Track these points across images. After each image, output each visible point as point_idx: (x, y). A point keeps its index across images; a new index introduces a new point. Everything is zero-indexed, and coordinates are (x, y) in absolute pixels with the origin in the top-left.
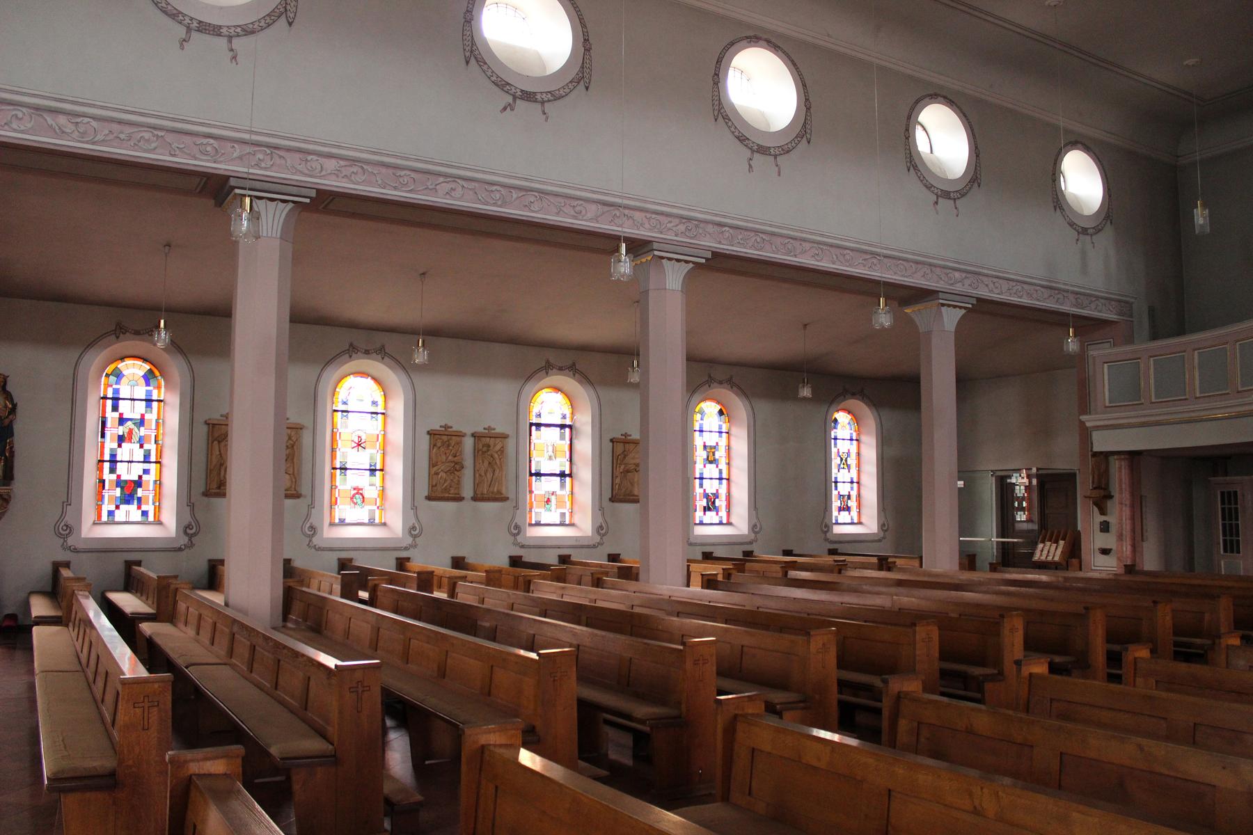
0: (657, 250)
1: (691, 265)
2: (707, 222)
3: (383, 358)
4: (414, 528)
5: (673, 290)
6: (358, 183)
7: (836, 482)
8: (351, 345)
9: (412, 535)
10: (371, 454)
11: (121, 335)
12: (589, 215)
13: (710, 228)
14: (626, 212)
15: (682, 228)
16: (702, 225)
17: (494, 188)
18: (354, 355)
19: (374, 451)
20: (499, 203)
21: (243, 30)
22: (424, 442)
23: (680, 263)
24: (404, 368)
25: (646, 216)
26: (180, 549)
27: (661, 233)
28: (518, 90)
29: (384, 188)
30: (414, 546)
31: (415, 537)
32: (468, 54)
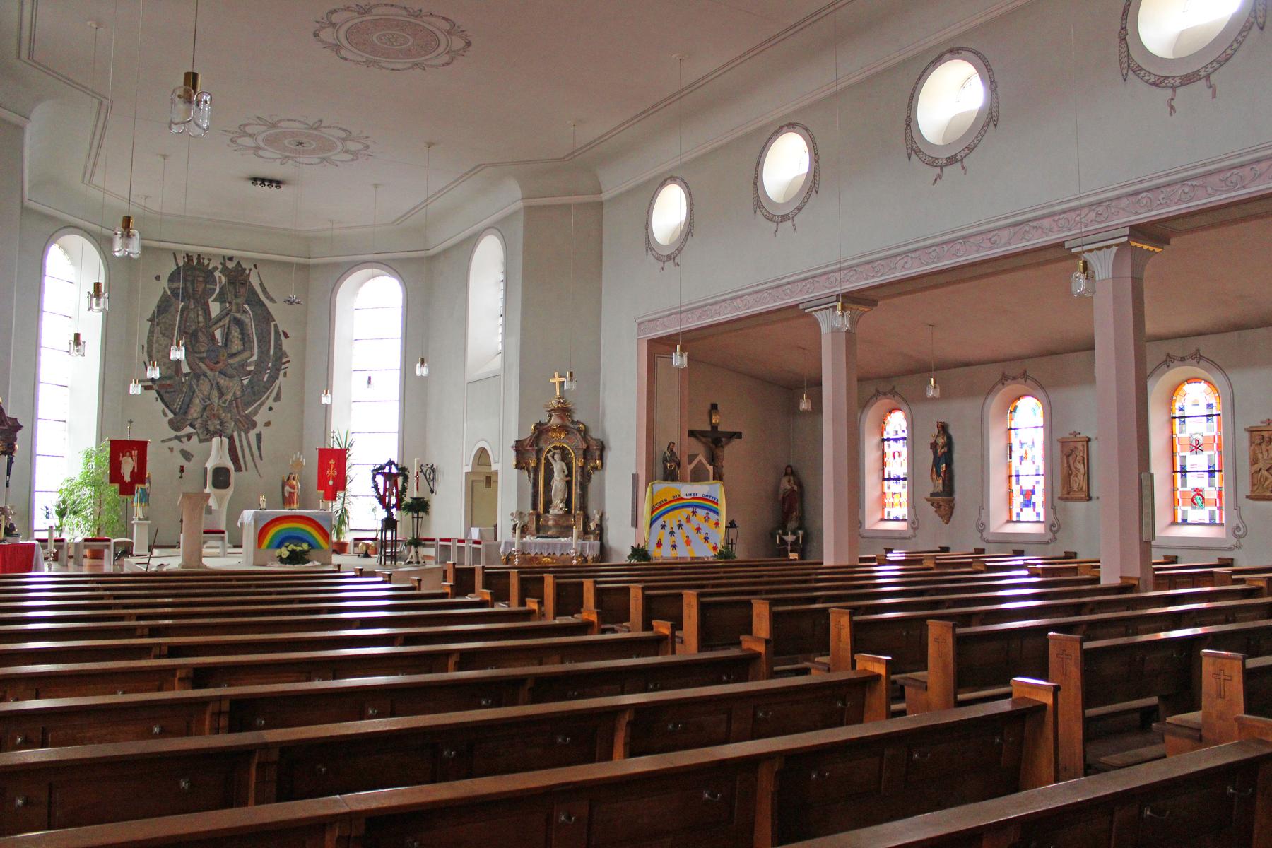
0: (1074, 247)
1: (1115, 249)
2: (1118, 198)
3: (1198, 362)
4: (1238, 528)
5: (1104, 280)
6: (854, 282)
7: (1017, 476)
8: (1168, 355)
9: (1236, 536)
10: (1209, 456)
11: (1171, 363)
12: (1003, 241)
13: (1124, 202)
14: (1035, 224)
15: (1092, 215)
16: (1114, 203)
17: (931, 250)
18: (1006, 383)
19: (1211, 453)
20: (935, 260)
21: (1218, 62)
22: (1244, 439)
23: (1102, 251)
24: (1219, 368)
25: (1054, 220)
26: (1047, 543)
27: (1070, 230)
28: (944, 160)
29: (867, 279)
30: (1238, 547)
31: (1239, 537)
32: (909, 151)
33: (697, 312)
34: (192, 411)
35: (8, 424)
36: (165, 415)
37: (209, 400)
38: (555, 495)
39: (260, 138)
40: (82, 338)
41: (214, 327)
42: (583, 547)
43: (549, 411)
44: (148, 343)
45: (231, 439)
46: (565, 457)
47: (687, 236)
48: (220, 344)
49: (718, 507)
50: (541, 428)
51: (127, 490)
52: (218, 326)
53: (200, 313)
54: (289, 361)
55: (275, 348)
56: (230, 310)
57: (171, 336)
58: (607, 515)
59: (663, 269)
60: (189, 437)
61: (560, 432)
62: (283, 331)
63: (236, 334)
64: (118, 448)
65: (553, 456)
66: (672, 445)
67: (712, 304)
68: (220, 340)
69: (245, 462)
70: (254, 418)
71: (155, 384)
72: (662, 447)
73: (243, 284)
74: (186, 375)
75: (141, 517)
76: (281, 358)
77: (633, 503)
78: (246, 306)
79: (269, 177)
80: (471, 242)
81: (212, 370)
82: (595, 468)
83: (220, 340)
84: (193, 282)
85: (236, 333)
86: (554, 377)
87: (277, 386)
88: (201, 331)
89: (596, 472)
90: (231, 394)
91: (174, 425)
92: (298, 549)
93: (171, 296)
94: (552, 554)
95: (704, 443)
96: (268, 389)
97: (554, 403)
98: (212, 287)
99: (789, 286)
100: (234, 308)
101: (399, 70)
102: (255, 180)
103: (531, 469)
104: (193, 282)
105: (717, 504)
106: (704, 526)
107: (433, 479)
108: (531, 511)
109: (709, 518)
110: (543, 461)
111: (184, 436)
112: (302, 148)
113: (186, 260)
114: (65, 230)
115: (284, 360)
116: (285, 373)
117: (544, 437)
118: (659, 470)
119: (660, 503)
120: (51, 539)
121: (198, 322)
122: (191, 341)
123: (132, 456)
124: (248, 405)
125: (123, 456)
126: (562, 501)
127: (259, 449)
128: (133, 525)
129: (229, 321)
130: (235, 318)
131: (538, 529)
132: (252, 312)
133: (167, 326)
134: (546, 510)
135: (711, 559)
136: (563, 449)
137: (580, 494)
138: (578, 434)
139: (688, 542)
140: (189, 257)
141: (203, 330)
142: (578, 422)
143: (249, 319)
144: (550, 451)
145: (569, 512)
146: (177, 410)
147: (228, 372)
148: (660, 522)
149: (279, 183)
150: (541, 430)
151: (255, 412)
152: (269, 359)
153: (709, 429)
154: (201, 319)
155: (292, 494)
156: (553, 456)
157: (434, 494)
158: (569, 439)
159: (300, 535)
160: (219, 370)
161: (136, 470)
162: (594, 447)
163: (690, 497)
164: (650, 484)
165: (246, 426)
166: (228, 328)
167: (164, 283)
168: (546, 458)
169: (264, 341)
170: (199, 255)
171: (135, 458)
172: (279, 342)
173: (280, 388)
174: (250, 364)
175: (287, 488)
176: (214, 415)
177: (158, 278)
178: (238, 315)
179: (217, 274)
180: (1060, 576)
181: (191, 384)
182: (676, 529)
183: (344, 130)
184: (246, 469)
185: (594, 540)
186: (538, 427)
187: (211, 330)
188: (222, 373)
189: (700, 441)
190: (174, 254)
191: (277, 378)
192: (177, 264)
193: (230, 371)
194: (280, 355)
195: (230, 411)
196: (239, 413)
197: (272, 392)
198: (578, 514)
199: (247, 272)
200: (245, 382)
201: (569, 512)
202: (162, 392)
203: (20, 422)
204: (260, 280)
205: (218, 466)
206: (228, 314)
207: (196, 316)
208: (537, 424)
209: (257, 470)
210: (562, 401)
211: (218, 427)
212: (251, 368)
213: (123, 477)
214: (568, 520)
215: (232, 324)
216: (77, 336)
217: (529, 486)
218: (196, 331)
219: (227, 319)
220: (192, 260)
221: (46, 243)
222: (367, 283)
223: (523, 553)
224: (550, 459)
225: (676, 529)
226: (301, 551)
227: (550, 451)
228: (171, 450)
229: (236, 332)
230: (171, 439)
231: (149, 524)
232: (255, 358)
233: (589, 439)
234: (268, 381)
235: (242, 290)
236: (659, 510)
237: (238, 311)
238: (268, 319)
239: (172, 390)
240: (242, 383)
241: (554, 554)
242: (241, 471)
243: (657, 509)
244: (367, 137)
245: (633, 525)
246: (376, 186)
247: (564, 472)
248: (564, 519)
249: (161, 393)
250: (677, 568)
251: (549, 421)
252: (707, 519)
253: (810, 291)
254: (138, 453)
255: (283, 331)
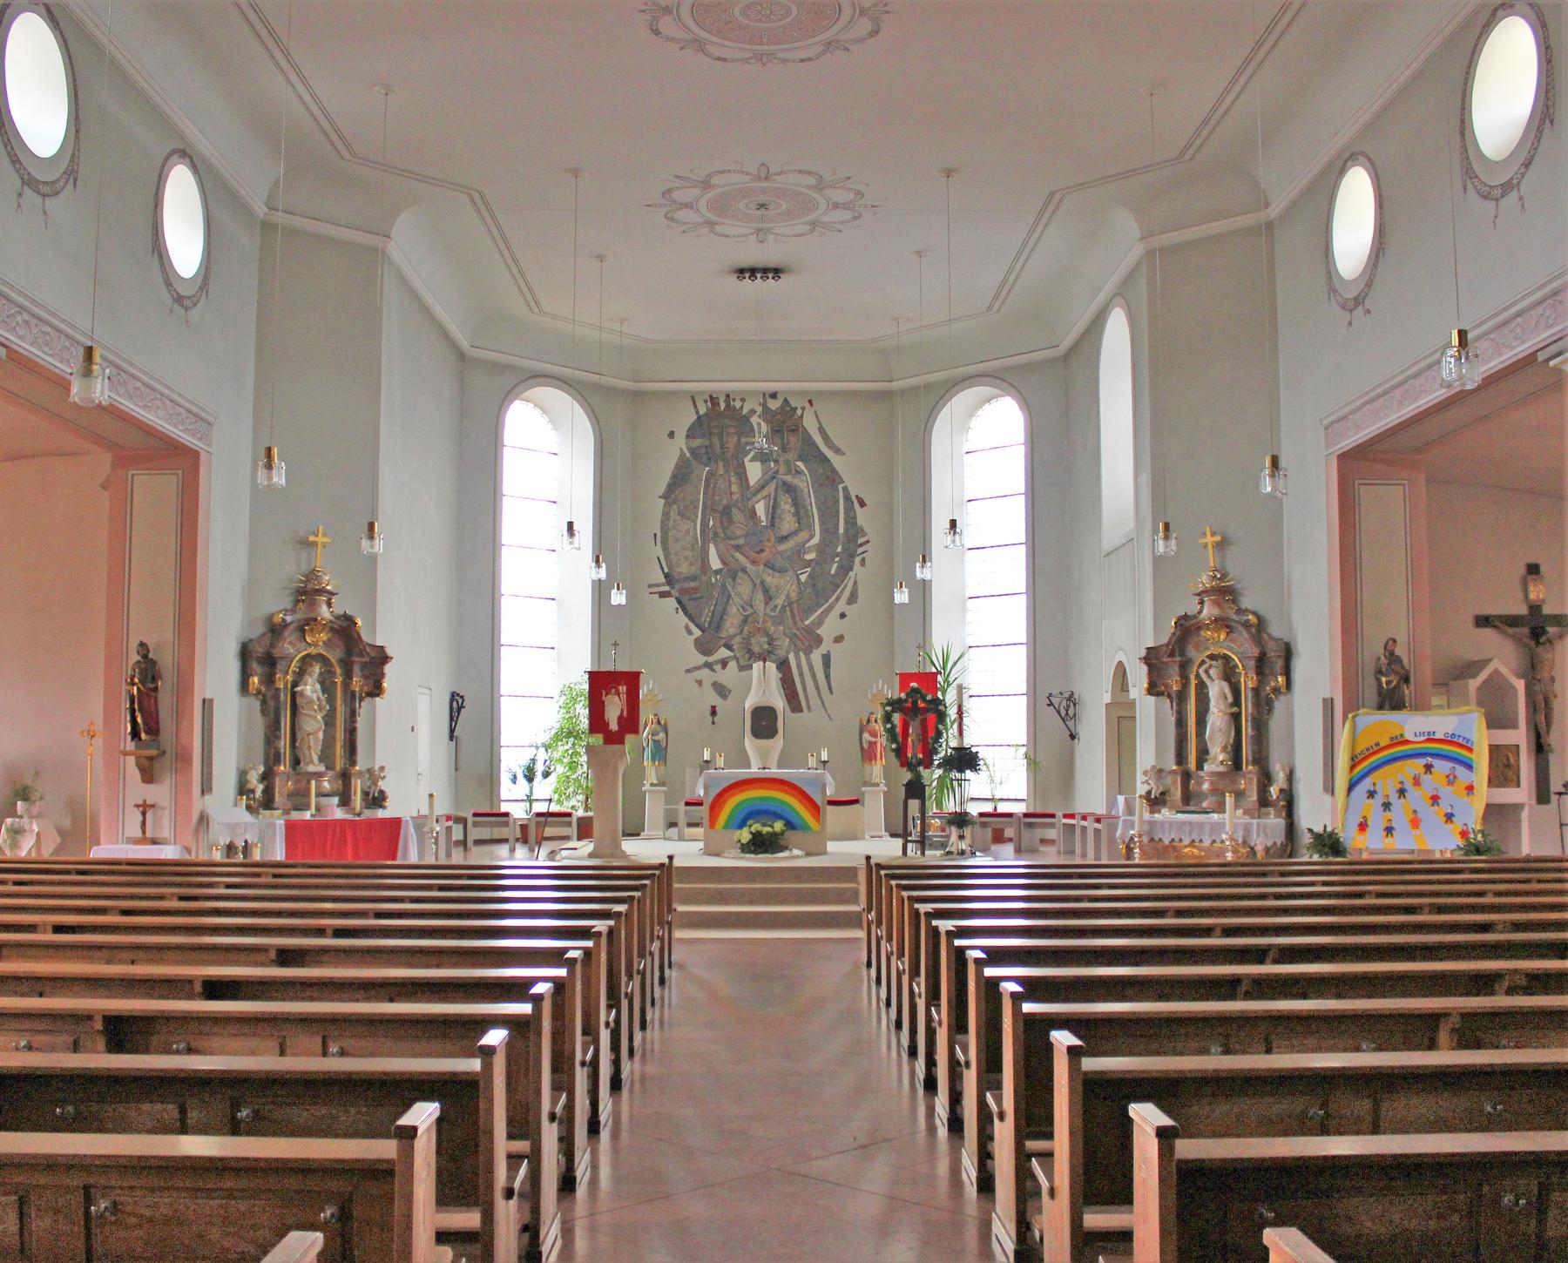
33: (1398, 394)
34: (727, 624)
35: (368, 654)
36: (689, 632)
37: (751, 606)
38: (1210, 738)
39: (702, 205)
40: (575, 527)
41: (755, 499)
42: (1247, 829)
43: (1198, 595)
44: (662, 529)
45: (783, 666)
46: (1229, 675)
47: (1377, 256)
48: (764, 524)
49: (1473, 756)
50: (1187, 624)
51: (614, 739)
52: (759, 496)
53: (733, 479)
54: (868, 542)
55: (846, 522)
56: (777, 472)
57: (693, 517)
58: (1299, 773)
59: (1350, 323)
60: (724, 663)
61: (1217, 630)
62: (857, 496)
63: (787, 507)
64: (600, 682)
65: (1207, 672)
66: (1391, 643)
67: (1414, 377)
68: (763, 518)
69: (806, 697)
70: (818, 632)
71: (673, 588)
72: (1373, 649)
73: (793, 431)
74: (717, 572)
75: (655, 782)
76: (855, 537)
77: (1325, 751)
78: (800, 464)
79: (760, 265)
80: (1098, 323)
81: (754, 562)
82: (1276, 690)
83: (763, 518)
84: (720, 435)
85: (786, 505)
87: (852, 579)
88: (735, 506)
89: (1282, 698)
90: (783, 597)
91: (704, 647)
92: (766, 829)
93: (691, 459)
94: (1177, 839)
95: (1512, 637)
96: (838, 587)
97: (1205, 580)
98: (748, 440)
99: (1519, 320)
100: (782, 469)
101: (810, 59)
102: (741, 272)
103: (1174, 695)
104: (720, 435)
105: (1470, 750)
106: (1445, 792)
107: (1075, 715)
108: (1174, 767)
109: (1455, 777)
110: (1193, 682)
111: (716, 662)
112: (765, 212)
113: (709, 404)
114: (533, 381)
115: (860, 541)
116: (863, 560)
117: (1195, 639)
118: (1371, 695)
119: (1368, 749)
120: (432, 817)
121: (731, 494)
122: (722, 523)
123: (618, 695)
124: (810, 611)
125: (607, 694)
126: (1224, 749)
127: (828, 677)
128: (645, 792)
129: (776, 488)
130: (784, 483)
131: (1187, 798)
132: (809, 470)
133: (688, 503)
134: (1200, 767)
135: (1448, 855)
136: (1226, 658)
137: (1252, 736)
138: (1244, 632)
139: (1415, 823)
140: (713, 400)
141: (740, 505)
142: (1247, 611)
143: (804, 483)
144: (1203, 662)
145: (1237, 764)
146: (706, 625)
147: (777, 565)
148: (1366, 785)
149: (777, 272)
150: (1187, 629)
151: (820, 622)
152: (838, 539)
153: (1523, 610)
154: (735, 488)
155: (872, 745)
156: (1207, 672)
157: (1076, 740)
158: (1233, 641)
159: (773, 809)
160: (763, 561)
161: (625, 714)
162: (1273, 650)
163: (1422, 738)
164: (1350, 716)
165: (807, 643)
166: (775, 499)
167: (681, 441)
168: (1198, 676)
169: (829, 514)
170: (728, 396)
171: (624, 697)
172: (852, 514)
173: (855, 582)
174: (810, 550)
175: (866, 736)
176: (759, 629)
177: (671, 435)
178: (788, 478)
179: (754, 420)
181: (724, 586)
182: (1394, 798)
183: (809, 173)
184: (809, 707)
185: (1275, 817)
186: (1182, 622)
187: (750, 504)
188: (770, 566)
189: (1502, 632)
190: (693, 397)
191: (851, 569)
192: (697, 412)
193: (779, 562)
194: (854, 531)
195: (781, 622)
196: (795, 623)
197: (842, 592)
198: (1250, 772)
199: (799, 412)
200: (803, 578)
201: (1237, 764)
202: (685, 599)
203: (389, 652)
204: (820, 423)
205: (758, 705)
206: (774, 478)
207: (727, 484)
208: (1180, 618)
209: (826, 710)
210: (1219, 576)
211: (766, 646)
212: (811, 556)
213: (608, 724)
215: (780, 492)
216: (570, 525)
217: (1172, 719)
218: (727, 508)
219: (773, 486)
220: (718, 404)
221: (503, 402)
222: (980, 412)
223: (1152, 840)
224: (1204, 676)
225: (1394, 798)
226: (768, 833)
227: (1203, 662)
228: (700, 683)
229: (786, 503)
230: (698, 668)
231: (665, 792)
232: (816, 540)
233: (1265, 636)
234: (837, 573)
235: (793, 440)
236: (1364, 764)
237: (789, 472)
238: (834, 481)
239: (698, 595)
240: (798, 579)
241: (1201, 841)
242: (802, 711)
243: (1360, 762)
244: (849, 178)
245: (1326, 790)
246: (919, 254)
247: (1226, 698)
248: (1227, 780)
249: (683, 601)
250: (1271, 873)
252: (1451, 779)
253: (1551, 322)
254: (627, 689)
255: (857, 496)
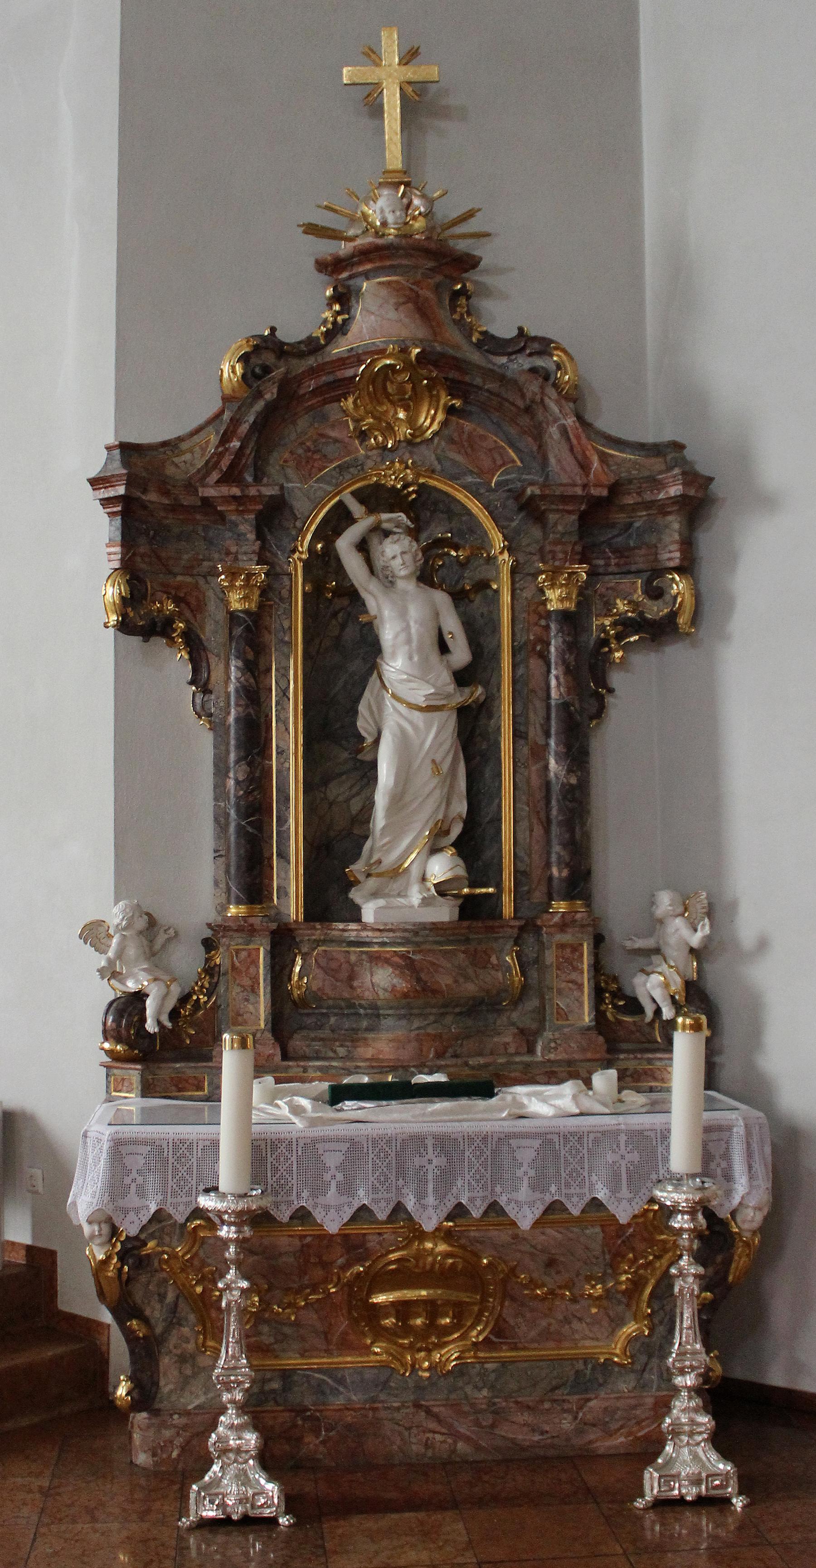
86: (372, 55)
158: (469, 445)
180: (498, 820)
214: (480, 960)
247: (443, 648)
251: (337, 331)
